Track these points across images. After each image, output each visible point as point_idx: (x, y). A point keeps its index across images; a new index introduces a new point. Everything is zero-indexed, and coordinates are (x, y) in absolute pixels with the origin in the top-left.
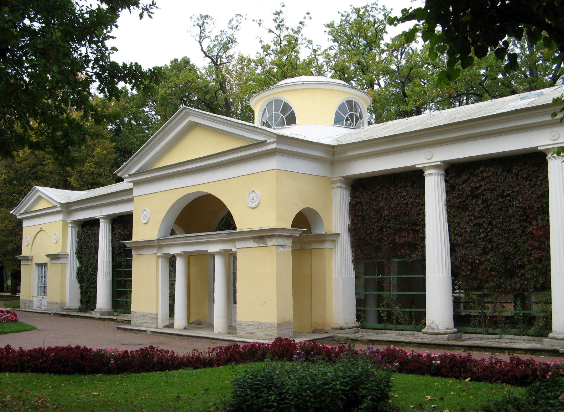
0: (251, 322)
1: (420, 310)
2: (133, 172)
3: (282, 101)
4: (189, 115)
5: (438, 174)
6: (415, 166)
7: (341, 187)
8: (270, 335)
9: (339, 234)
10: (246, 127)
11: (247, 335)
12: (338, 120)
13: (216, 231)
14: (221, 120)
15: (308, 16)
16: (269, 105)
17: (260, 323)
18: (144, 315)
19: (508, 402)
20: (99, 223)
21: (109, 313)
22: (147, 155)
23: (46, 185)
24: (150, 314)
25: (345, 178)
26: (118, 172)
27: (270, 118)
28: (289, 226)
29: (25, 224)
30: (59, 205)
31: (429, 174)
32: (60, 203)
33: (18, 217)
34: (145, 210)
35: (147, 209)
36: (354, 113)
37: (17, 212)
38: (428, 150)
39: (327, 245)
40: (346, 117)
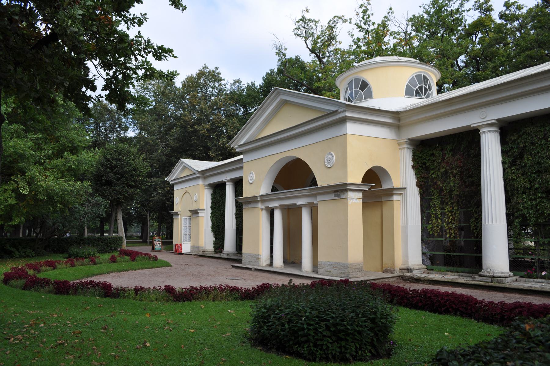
0: (329, 262)
1: (479, 255)
2: (242, 143)
3: (361, 79)
4: (280, 94)
5: (493, 131)
6: (470, 125)
7: (407, 148)
8: (343, 273)
9: (405, 188)
10: (317, 99)
11: (326, 273)
12: (409, 92)
13: (309, 187)
14: (302, 96)
15: (391, 11)
16: (350, 84)
17: (336, 263)
18: (251, 256)
19: (382, 356)
20: (226, 186)
21: (234, 254)
22: (251, 129)
23: (194, 158)
24: (255, 255)
25: (410, 140)
26: (231, 144)
27: (351, 94)
28: (359, 181)
29: (176, 188)
30: (197, 173)
31: (484, 132)
32: (198, 171)
33: (171, 183)
34: (251, 173)
35: (253, 172)
36: (423, 85)
37: (170, 179)
38: (483, 110)
39: (395, 198)
40: (415, 89)
